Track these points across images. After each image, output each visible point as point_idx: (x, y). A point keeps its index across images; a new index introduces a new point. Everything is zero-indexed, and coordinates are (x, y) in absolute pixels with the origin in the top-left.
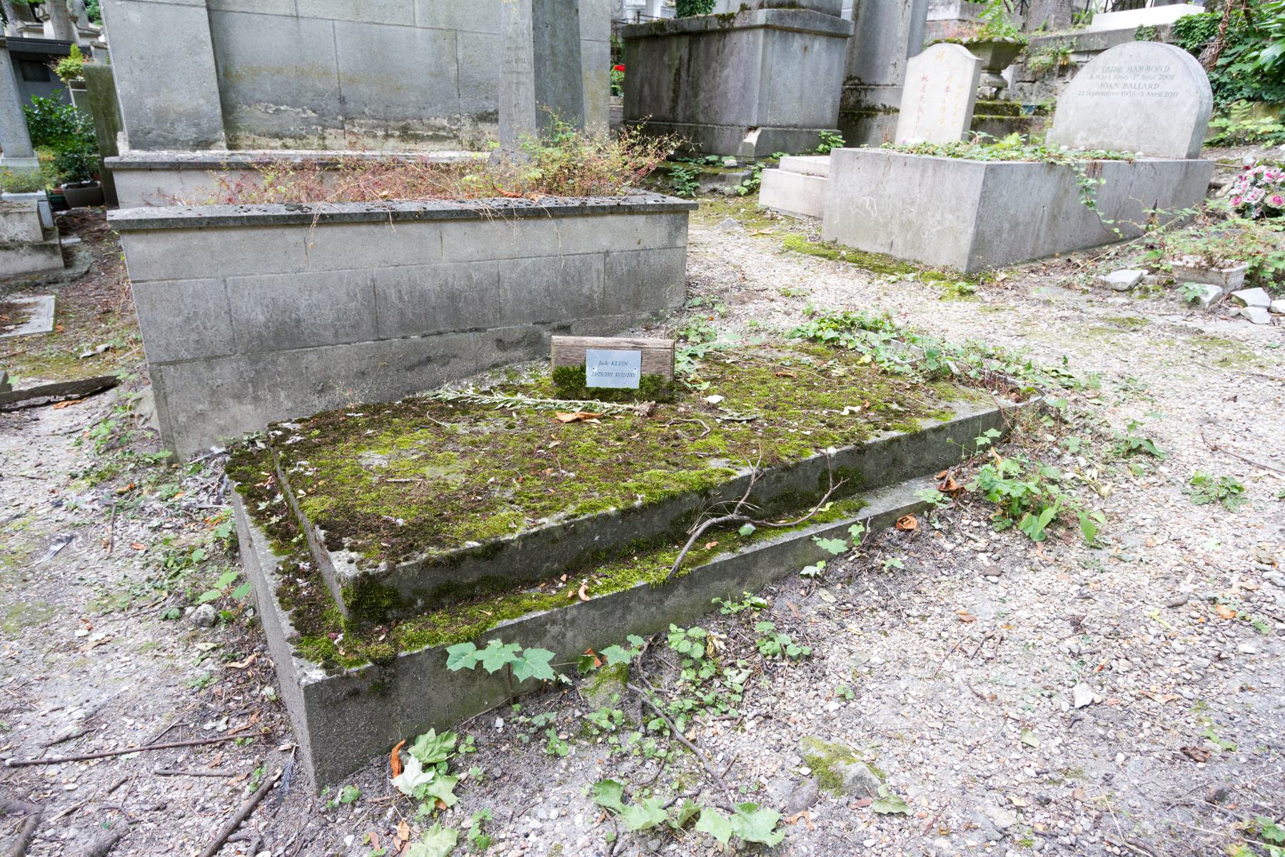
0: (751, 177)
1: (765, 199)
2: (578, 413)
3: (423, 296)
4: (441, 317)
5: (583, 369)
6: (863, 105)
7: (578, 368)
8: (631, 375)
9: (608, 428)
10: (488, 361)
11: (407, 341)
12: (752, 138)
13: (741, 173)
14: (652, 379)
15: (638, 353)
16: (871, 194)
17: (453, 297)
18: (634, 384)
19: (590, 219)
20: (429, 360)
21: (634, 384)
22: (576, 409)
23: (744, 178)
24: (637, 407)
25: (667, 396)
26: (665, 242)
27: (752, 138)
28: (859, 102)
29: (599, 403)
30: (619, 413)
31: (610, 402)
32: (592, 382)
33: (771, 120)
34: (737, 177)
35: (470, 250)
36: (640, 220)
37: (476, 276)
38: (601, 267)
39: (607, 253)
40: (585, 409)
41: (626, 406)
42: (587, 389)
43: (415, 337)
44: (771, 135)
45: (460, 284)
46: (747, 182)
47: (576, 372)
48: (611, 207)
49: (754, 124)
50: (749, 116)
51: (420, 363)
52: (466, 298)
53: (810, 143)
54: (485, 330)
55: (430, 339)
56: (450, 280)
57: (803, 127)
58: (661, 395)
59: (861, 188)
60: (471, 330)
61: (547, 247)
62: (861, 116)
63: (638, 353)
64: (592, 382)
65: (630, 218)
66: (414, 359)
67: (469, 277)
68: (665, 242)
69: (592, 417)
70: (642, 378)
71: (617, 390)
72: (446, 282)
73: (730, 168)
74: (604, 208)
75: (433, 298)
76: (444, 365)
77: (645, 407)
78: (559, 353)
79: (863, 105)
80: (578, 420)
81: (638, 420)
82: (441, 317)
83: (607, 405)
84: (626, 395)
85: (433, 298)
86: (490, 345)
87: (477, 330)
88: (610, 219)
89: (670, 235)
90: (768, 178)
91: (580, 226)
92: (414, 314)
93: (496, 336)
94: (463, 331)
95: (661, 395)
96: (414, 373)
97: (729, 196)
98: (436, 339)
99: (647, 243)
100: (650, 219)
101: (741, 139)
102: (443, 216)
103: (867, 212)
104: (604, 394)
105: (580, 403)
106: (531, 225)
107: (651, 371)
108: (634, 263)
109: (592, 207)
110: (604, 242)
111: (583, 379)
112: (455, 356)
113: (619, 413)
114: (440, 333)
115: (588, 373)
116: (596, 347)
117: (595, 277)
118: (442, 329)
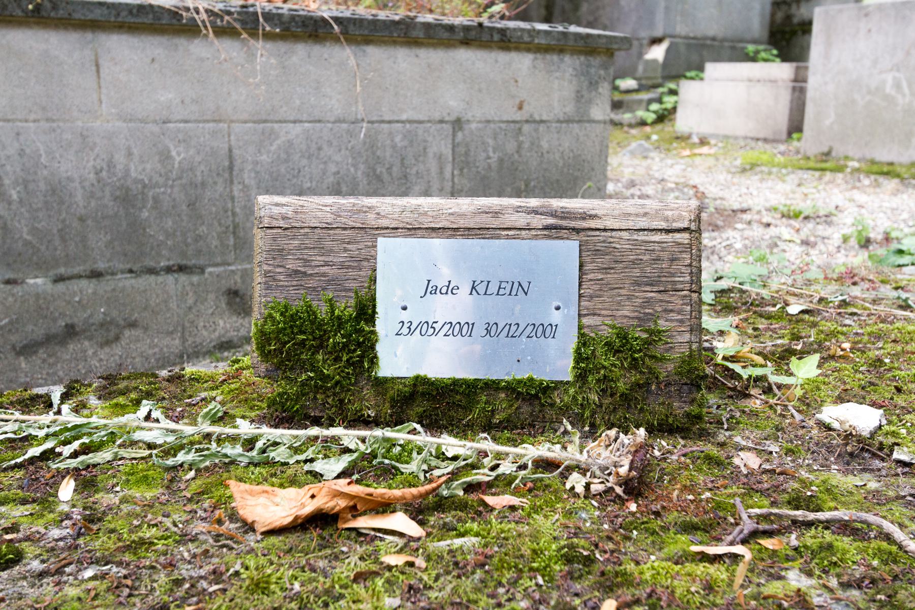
0: (660, 101)
1: (683, 122)
2: (331, 486)
3: (57, 192)
4: (98, 240)
5: (366, 311)
6: (796, 20)
7: (346, 307)
8: (546, 330)
9: (457, 565)
10: (207, 336)
11: (17, 290)
12: (657, 53)
13: (645, 96)
14: (621, 344)
15: (569, 248)
16: (897, 68)
17: (127, 198)
18: (556, 363)
19: (423, 52)
20: (71, 332)
21: (556, 363)
22: (326, 465)
23: (650, 101)
24: (572, 453)
25: (680, 408)
26: (570, 109)
27: (657, 53)
28: (789, 17)
29: (423, 438)
30: (503, 483)
31: (463, 431)
32: (399, 357)
33: (681, 29)
34: (640, 102)
35: (166, 96)
36: (522, 62)
37: (178, 155)
38: (447, 152)
39: (458, 124)
40: (361, 468)
41: (531, 451)
42: (381, 384)
43: (37, 282)
44: (682, 49)
45: (140, 169)
46: (655, 107)
47: (340, 322)
48: (467, 29)
49: (658, 33)
50: (652, 25)
51: (49, 340)
52: (156, 200)
53: (734, 50)
54: (202, 270)
55: (75, 285)
56: (120, 159)
57: (723, 40)
58: (656, 406)
59: (875, 62)
60: (169, 270)
61: (333, 102)
62: (794, 33)
63: (569, 248)
64: (399, 357)
65: (503, 57)
66: (35, 330)
67: (165, 157)
68: (570, 109)
69: (384, 507)
70: (584, 340)
71: (491, 386)
72: (111, 165)
73: (628, 92)
74: (451, 28)
75: (79, 197)
76: (108, 343)
77: (609, 454)
78: (278, 253)
79: (796, 20)
80: (321, 520)
81: (589, 515)
82: (98, 240)
83: (451, 444)
84: (524, 407)
85: (79, 197)
86: (213, 302)
87: (181, 269)
88: (464, 55)
89: (579, 96)
90: (689, 90)
91: (403, 62)
92: (34, 231)
93: (225, 284)
94: (152, 271)
95: (656, 406)
96: (36, 360)
97: (631, 126)
98: (88, 287)
99: (535, 108)
100: (542, 61)
101: (640, 55)
102: (97, 14)
103: (887, 98)
104: (440, 404)
105: (349, 436)
106: (301, 54)
107: (620, 313)
108: (511, 146)
109: (427, 26)
110: (452, 101)
111: (366, 347)
112: (133, 325)
113: (503, 483)
114: (96, 275)
115: (384, 325)
116: (412, 231)
117: (434, 170)
118: (101, 266)
